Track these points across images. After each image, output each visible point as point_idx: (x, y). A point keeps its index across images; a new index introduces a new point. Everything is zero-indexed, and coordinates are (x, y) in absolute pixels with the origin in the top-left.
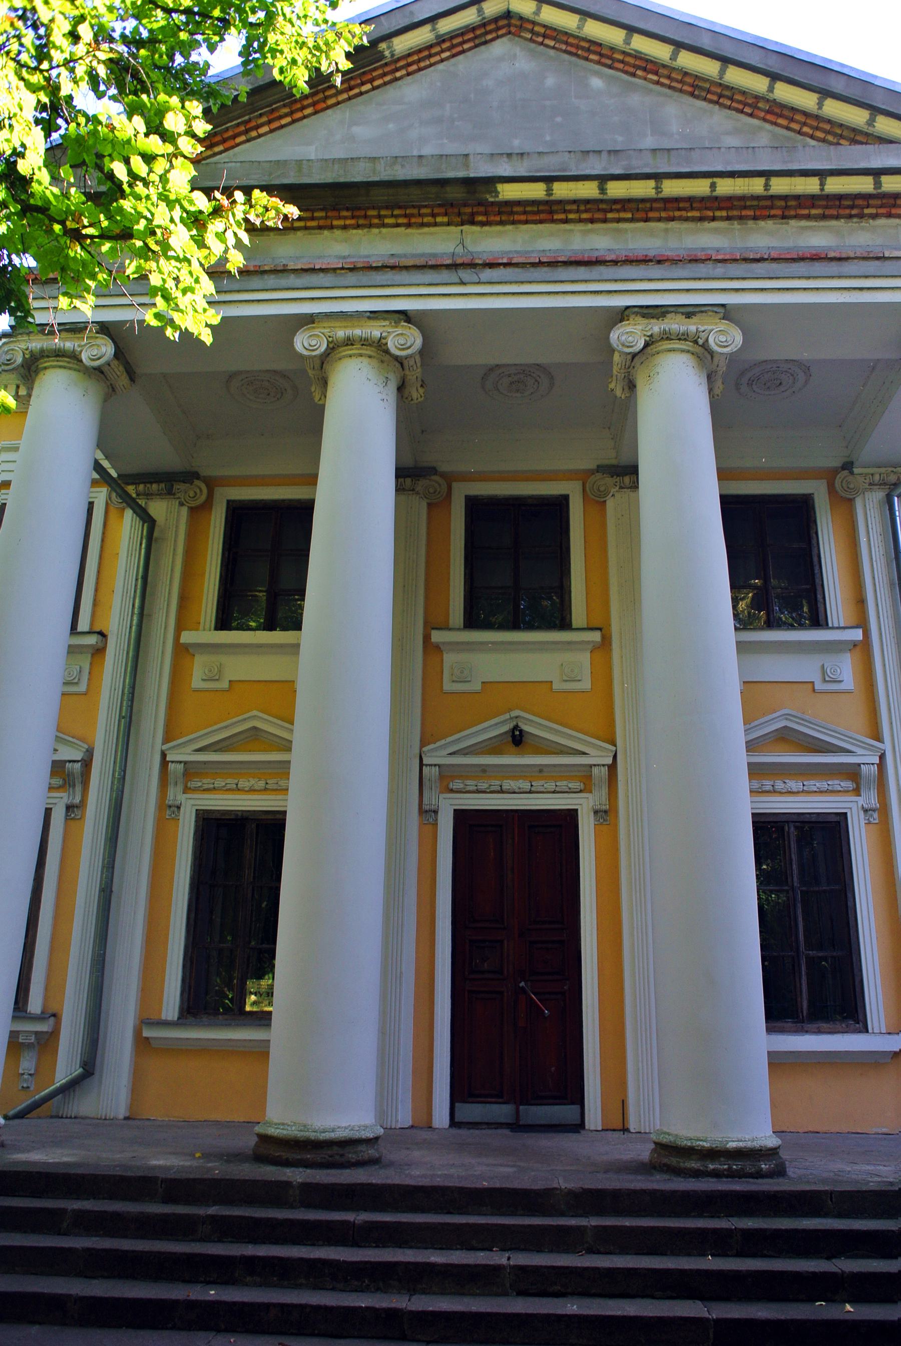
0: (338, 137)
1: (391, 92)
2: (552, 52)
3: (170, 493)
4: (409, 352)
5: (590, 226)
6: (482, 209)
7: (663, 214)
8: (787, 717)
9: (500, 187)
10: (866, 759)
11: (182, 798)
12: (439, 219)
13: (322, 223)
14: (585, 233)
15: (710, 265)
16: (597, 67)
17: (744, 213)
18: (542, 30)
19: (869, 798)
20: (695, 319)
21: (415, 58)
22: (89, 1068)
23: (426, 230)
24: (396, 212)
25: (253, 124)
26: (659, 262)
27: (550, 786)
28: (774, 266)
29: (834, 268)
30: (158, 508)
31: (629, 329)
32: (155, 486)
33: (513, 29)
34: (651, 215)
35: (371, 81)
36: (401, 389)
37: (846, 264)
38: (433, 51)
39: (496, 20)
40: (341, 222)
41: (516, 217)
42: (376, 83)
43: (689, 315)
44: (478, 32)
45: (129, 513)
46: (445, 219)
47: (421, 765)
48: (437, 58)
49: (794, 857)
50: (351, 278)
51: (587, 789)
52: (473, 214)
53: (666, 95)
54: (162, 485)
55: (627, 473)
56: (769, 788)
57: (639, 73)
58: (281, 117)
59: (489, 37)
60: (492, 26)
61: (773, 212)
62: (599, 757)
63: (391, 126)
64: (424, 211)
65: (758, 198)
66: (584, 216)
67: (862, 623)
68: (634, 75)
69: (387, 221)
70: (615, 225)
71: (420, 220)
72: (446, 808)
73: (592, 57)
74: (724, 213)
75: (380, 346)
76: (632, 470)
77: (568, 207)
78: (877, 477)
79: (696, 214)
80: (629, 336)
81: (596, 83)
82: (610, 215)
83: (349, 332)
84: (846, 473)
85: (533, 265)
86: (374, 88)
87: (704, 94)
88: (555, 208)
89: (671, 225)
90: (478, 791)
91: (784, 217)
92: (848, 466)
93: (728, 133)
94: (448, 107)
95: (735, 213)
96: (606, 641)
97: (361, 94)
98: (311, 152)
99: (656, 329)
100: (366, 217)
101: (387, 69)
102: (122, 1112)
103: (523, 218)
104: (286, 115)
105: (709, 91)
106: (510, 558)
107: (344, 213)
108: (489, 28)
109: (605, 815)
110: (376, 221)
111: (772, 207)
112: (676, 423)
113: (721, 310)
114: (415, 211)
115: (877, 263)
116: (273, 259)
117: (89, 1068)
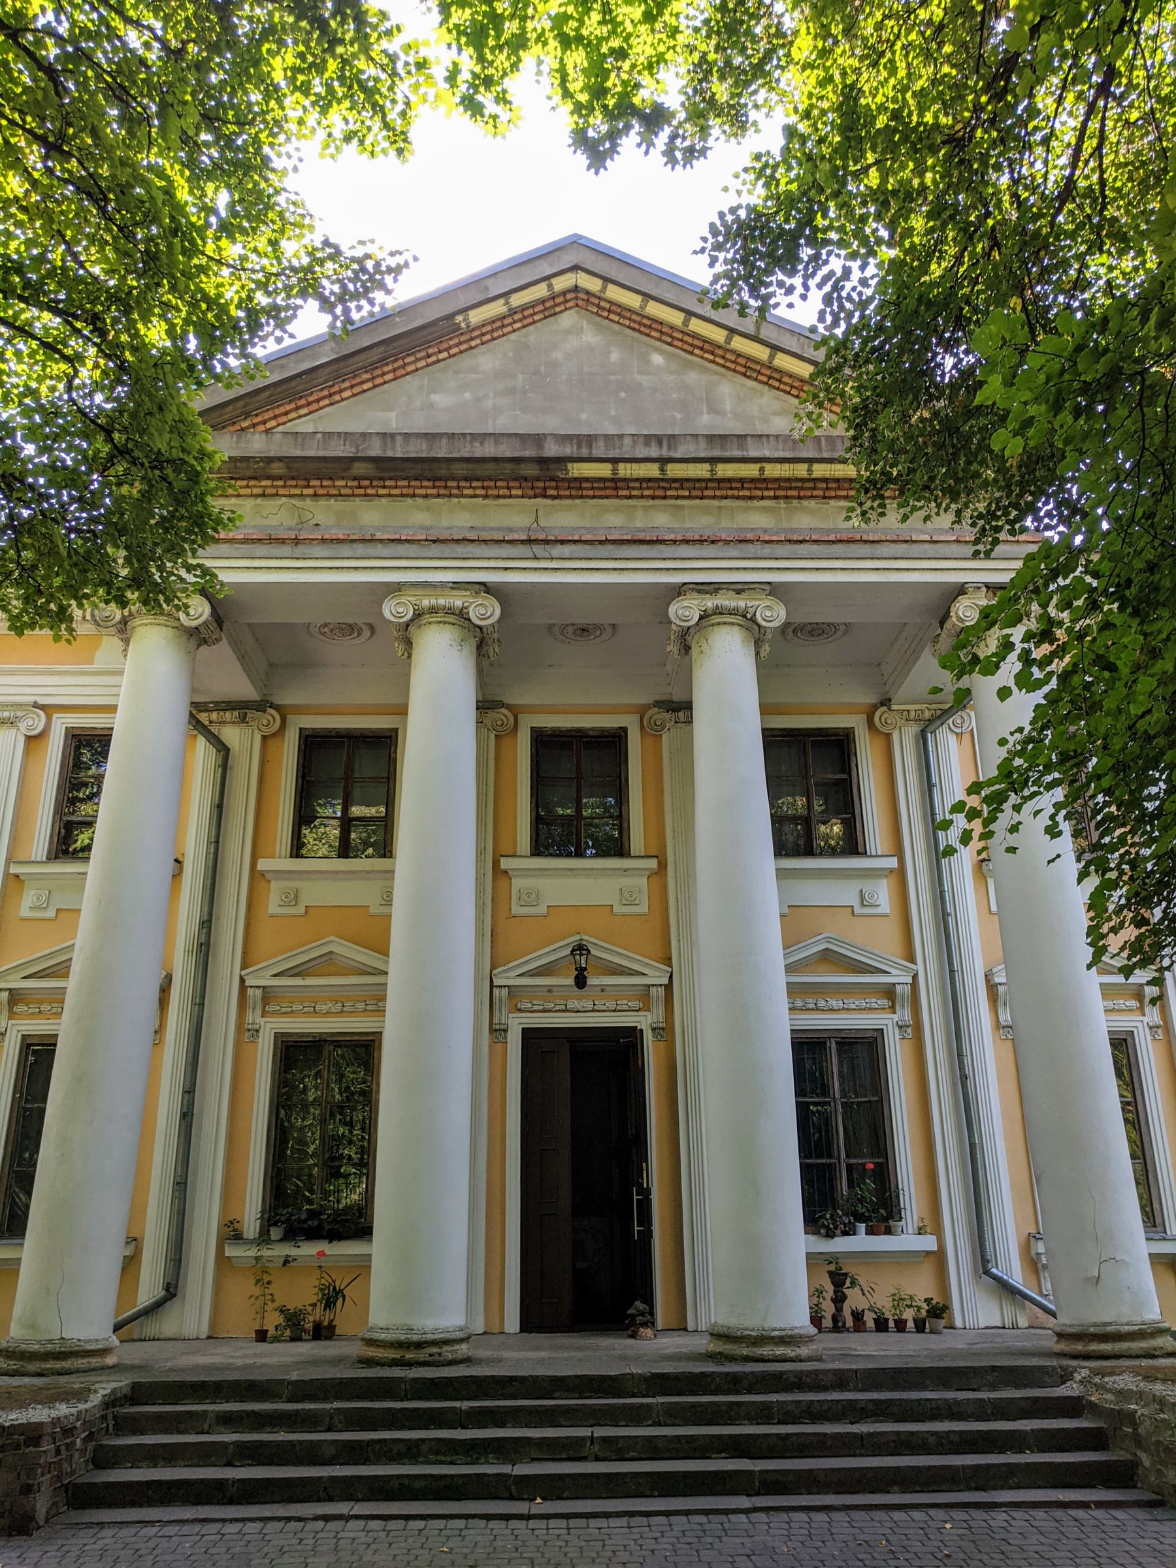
0: (418, 404)
1: (466, 361)
2: (616, 327)
3: (243, 719)
4: (490, 621)
5: (651, 502)
6: (553, 484)
7: (718, 493)
8: (828, 940)
9: (570, 466)
10: (899, 977)
12: (514, 492)
13: (405, 491)
14: (646, 509)
15: (758, 546)
16: (658, 343)
17: (790, 493)
18: (607, 306)
20: (744, 595)
21: (489, 328)
22: (171, 1291)
23: (502, 501)
24: (474, 484)
25: (336, 388)
26: (713, 542)
27: (611, 1005)
28: (815, 547)
29: (866, 550)
30: (232, 735)
31: (686, 603)
32: (228, 714)
33: (580, 303)
34: (706, 493)
35: (447, 350)
36: (479, 647)
37: (877, 546)
38: (506, 322)
39: (564, 293)
40: (423, 492)
41: (585, 493)
42: (453, 351)
43: (739, 592)
44: (548, 305)
45: (201, 741)
46: (520, 492)
47: (492, 986)
48: (510, 329)
49: (835, 1070)
50: (435, 550)
52: (545, 488)
53: (721, 375)
54: (236, 713)
55: (681, 709)
56: (811, 1006)
57: (697, 351)
58: (362, 383)
59: (557, 309)
60: (561, 299)
61: (815, 493)
62: (656, 976)
63: (467, 395)
64: (499, 484)
65: (802, 480)
66: (646, 493)
67: (899, 853)
68: (692, 353)
69: (466, 492)
70: (673, 502)
71: (495, 492)
72: (516, 1025)
73: (653, 334)
74: (771, 493)
75: (461, 616)
76: (688, 706)
77: (632, 485)
78: (913, 714)
79: (747, 493)
80: (686, 610)
81: (657, 359)
82: (669, 493)
83: (433, 601)
84: (884, 708)
85: (601, 542)
86: (450, 356)
87: (754, 375)
88: (619, 484)
89: (724, 502)
90: (544, 1011)
91: (824, 497)
92: (886, 702)
93: (775, 414)
94: (520, 377)
95: (782, 493)
96: (663, 866)
97: (438, 361)
98: (392, 421)
99: (710, 604)
100: (446, 487)
101: (462, 338)
102: (204, 1331)
103: (591, 493)
104: (368, 380)
105: (759, 372)
106: (577, 787)
107: (425, 483)
108: (558, 300)
109: (664, 1032)
110: (455, 491)
111: (814, 488)
112: (729, 687)
113: (767, 587)
114: (492, 484)
115: (905, 546)
116: (361, 527)
117: (171, 1291)
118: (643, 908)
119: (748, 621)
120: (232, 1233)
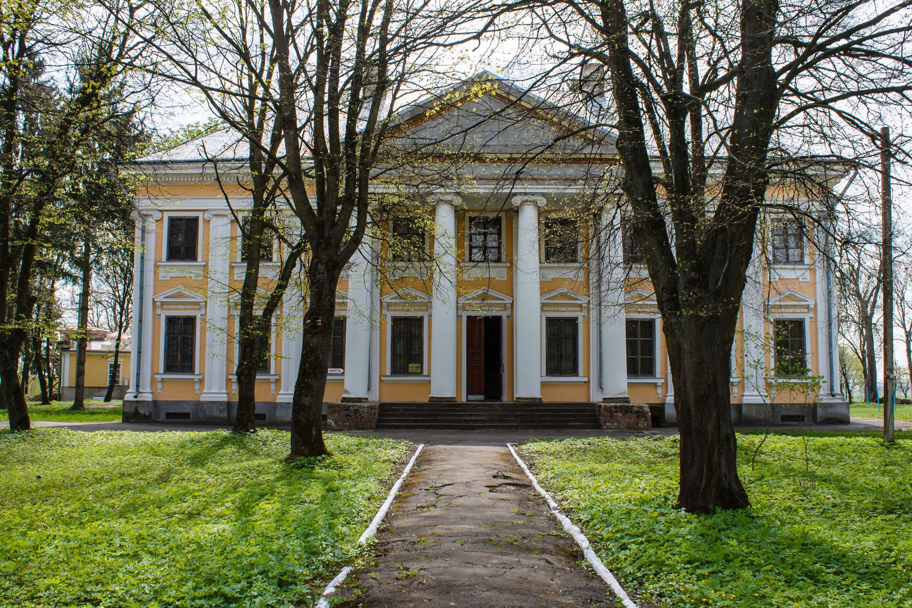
10: (811, 303)
11: (387, 313)
19: (585, 313)
51: (505, 310)
62: (508, 301)
72: (389, 315)
109: (511, 317)
118: (505, 279)
119: (535, 203)
120: (154, 373)
